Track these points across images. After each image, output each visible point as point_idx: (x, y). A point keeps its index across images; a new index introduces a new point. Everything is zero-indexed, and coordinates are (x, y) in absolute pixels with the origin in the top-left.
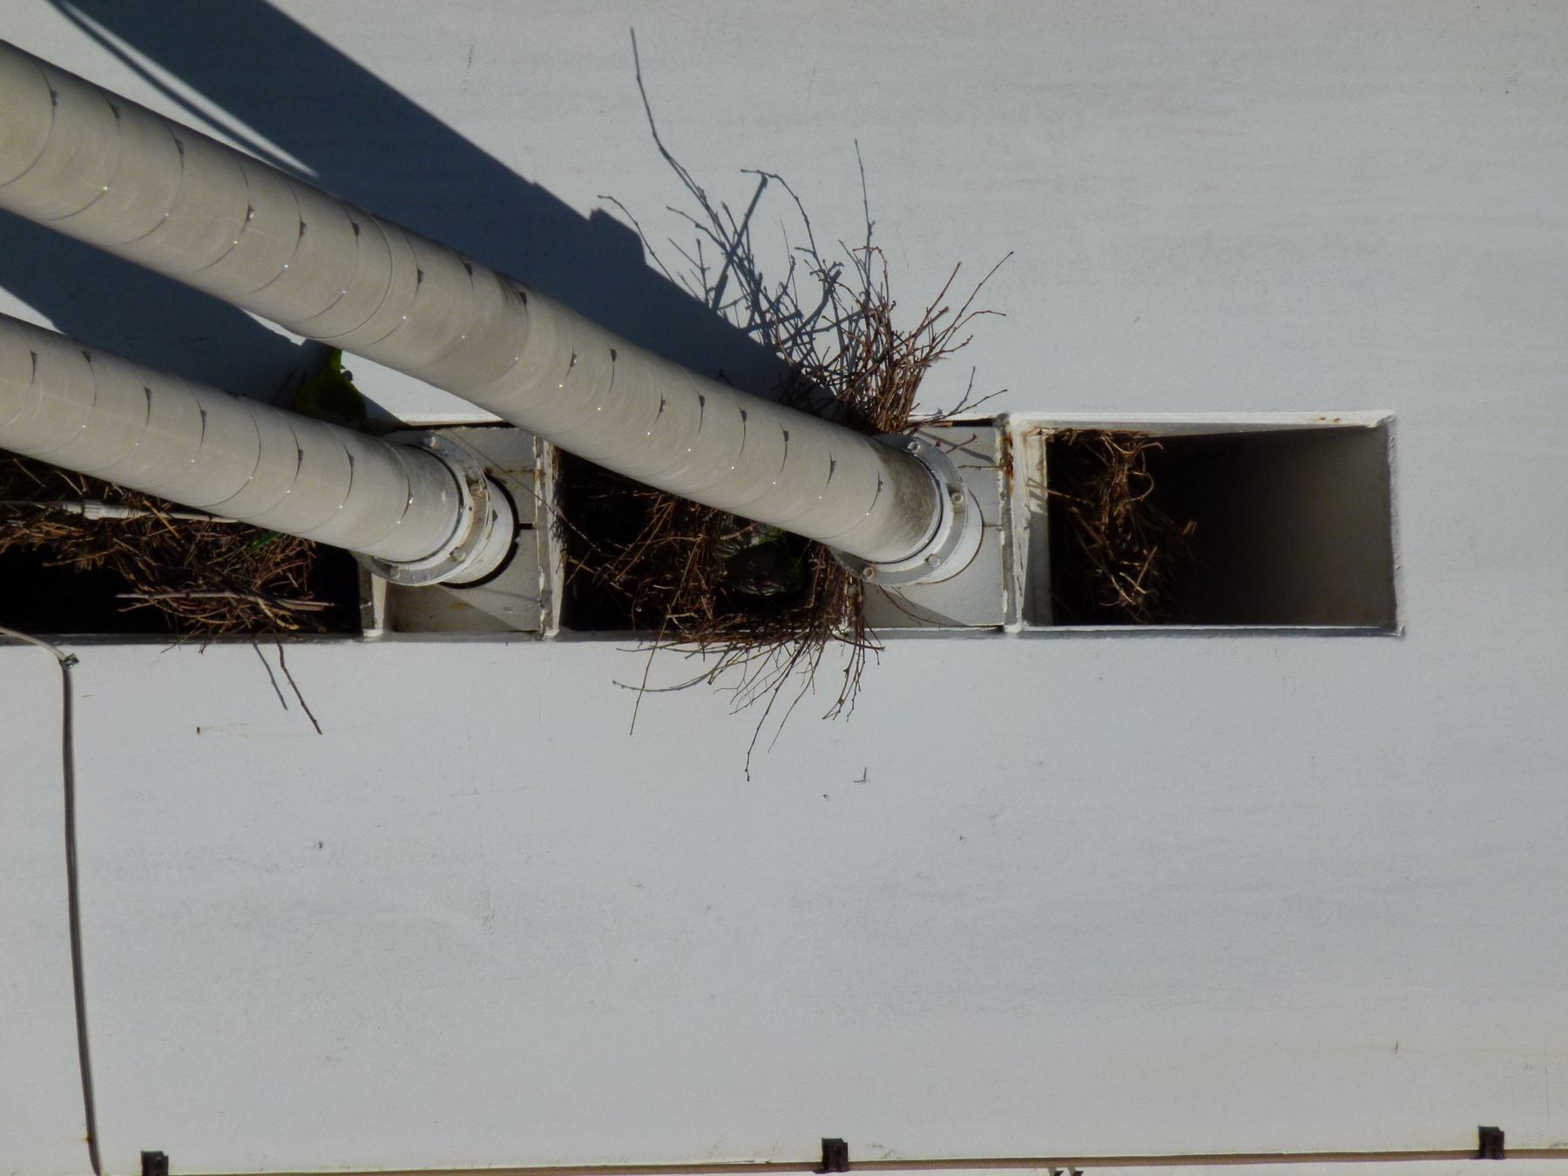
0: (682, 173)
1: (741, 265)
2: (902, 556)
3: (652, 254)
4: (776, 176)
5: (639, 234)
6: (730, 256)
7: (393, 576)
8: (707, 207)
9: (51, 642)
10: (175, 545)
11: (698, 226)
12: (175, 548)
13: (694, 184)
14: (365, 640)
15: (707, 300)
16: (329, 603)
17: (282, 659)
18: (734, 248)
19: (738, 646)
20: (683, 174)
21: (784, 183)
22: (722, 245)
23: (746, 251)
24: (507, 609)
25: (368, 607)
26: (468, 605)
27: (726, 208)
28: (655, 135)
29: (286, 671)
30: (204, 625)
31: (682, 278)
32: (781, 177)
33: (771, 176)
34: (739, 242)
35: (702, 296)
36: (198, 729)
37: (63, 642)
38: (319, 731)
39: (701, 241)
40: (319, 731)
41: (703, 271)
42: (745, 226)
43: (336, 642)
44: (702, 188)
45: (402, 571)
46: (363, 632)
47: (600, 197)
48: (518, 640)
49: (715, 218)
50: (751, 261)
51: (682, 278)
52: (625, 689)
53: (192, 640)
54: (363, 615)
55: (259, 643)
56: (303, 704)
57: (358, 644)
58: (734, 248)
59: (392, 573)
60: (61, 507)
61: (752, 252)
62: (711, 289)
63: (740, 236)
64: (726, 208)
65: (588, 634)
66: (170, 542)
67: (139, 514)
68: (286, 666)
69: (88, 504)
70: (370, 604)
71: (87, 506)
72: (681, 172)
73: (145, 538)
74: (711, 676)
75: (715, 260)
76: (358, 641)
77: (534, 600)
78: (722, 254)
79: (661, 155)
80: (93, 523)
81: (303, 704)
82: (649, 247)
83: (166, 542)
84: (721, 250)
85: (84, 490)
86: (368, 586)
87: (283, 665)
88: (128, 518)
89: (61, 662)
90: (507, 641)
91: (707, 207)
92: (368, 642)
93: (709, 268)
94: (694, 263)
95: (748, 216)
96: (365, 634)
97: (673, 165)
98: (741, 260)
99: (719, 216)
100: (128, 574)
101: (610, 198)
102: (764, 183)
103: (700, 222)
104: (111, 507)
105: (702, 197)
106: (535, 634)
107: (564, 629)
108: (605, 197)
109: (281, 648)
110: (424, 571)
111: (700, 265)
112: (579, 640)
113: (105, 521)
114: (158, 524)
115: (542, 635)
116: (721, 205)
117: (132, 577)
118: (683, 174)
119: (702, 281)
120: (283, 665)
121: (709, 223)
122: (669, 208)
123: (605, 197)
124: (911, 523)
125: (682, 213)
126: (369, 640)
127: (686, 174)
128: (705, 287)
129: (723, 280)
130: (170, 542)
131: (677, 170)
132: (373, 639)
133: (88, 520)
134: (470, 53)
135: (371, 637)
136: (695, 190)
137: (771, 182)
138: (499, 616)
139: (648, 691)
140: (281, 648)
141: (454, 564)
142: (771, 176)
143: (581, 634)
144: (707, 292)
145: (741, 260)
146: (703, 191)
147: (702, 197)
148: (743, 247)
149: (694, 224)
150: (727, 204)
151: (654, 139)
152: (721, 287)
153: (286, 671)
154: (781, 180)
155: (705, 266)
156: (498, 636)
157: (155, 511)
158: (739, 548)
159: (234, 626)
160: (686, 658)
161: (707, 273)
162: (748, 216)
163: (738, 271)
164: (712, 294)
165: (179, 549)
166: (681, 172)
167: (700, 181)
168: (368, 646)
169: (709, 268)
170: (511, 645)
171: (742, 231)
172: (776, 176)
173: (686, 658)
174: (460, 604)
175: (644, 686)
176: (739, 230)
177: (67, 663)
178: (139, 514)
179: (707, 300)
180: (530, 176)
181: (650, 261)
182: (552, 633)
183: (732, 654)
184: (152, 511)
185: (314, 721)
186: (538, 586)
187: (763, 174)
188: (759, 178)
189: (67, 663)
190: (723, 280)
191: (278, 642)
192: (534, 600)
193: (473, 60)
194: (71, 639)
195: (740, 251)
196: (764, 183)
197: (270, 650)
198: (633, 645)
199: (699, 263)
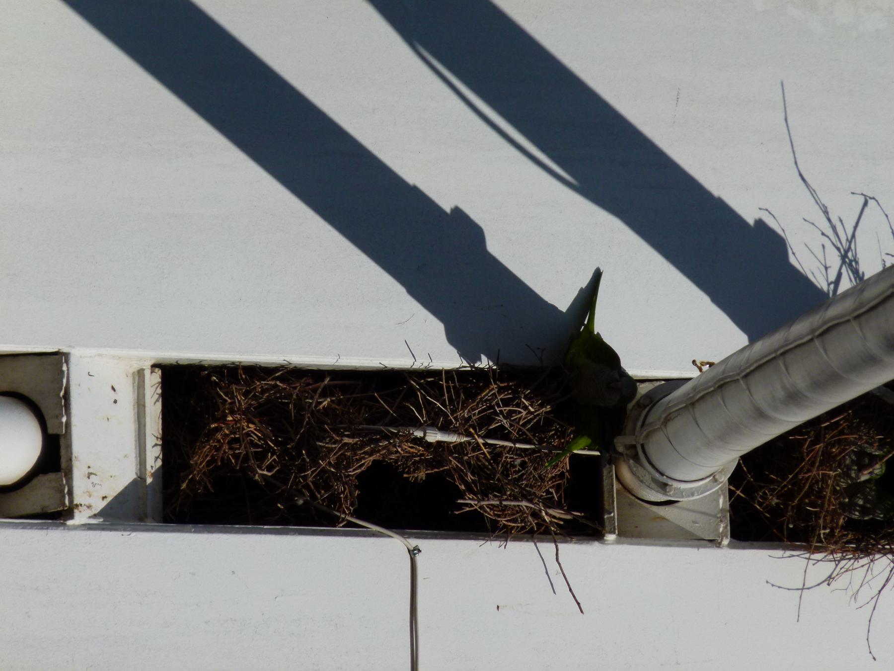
0: (813, 192)
1: (850, 265)
2: (653, 499)
3: (794, 254)
4: (873, 198)
5: (785, 238)
6: (844, 257)
7: (669, 492)
8: (829, 220)
9: (402, 535)
10: (487, 464)
11: (823, 234)
12: (486, 467)
13: (820, 201)
14: (606, 542)
15: (828, 290)
16: (581, 513)
17: (557, 554)
18: (846, 252)
19: (847, 557)
20: (813, 193)
21: (878, 204)
22: (838, 249)
23: (854, 254)
24: (694, 522)
25: (611, 517)
26: (663, 518)
27: (841, 221)
28: (796, 163)
29: (559, 564)
30: (505, 526)
31: (813, 273)
32: (877, 199)
33: (871, 198)
34: (850, 248)
35: (825, 288)
36: (498, 607)
37: (410, 536)
38: (582, 612)
39: (825, 245)
40: (582, 612)
41: (826, 268)
42: (853, 236)
43: (587, 543)
44: (826, 205)
45: (675, 489)
46: (604, 536)
47: (760, 209)
48: (705, 547)
49: (834, 228)
50: (857, 263)
51: (813, 273)
52: (774, 587)
53: (497, 538)
54: (607, 523)
55: (537, 542)
56: (570, 590)
57: (602, 545)
58: (846, 252)
59: (668, 490)
60: (409, 432)
61: (858, 256)
62: (832, 283)
63: (850, 242)
64: (841, 221)
65: (747, 544)
66: (484, 461)
67: (464, 439)
68: (560, 560)
69: (428, 430)
70: (612, 515)
71: (427, 431)
72: (812, 191)
73: (466, 458)
74: (830, 579)
75: (834, 260)
76: (602, 543)
77: (715, 516)
78: (839, 256)
79: (799, 179)
80: (429, 445)
81: (570, 590)
82: (792, 249)
83: (480, 461)
84: (838, 253)
85: (425, 419)
86: (611, 500)
87: (557, 559)
88: (455, 442)
89: (409, 551)
90: (698, 547)
91: (829, 220)
92: (608, 544)
93: (830, 267)
94: (820, 261)
95: (855, 227)
96: (605, 538)
97: (809, 189)
98: (851, 261)
99: (837, 226)
100: (461, 485)
101: (767, 210)
102: (866, 204)
103: (824, 231)
104: (444, 433)
105: (826, 212)
106: (714, 543)
107: (732, 539)
108: (764, 209)
109: (557, 547)
110: (692, 488)
111: (824, 264)
112: (744, 548)
113: (439, 443)
114: (477, 447)
115: (720, 543)
116: (838, 219)
117: (463, 487)
118: (813, 193)
119: (826, 277)
120: (557, 559)
121: (829, 232)
122: (805, 220)
123: (764, 209)
124: (419, 480)
125: (813, 224)
126: (609, 542)
127: (816, 193)
128: (827, 281)
129: (839, 275)
130: (484, 461)
131: (810, 190)
132: (611, 542)
133: (426, 442)
134: (678, 95)
135: (611, 541)
136: (822, 207)
137: (871, 202)
138: (688, 528)
139: (808, 588)
140: (557, 547)
141: (715, 484)
142: (871, 198)
143: (743, 544)
144: (829, 285)
145: (851, 261)
146: (826, 207)
147: (826, 212)
148: (852, 251)
149: (821, 232)
150: (842, 218)
151: (795, 166)
152: (837, 282)
153: (559, 564)
154: (877, 201)
155: (828, 266)
156: (690, 543)
157: (476, 437)
158: (849, 482)
159: (523, 528)
160: (814, 565)
161: (829, 270)
162: (855, 227)
163: (849, 269)
164: (832, 286)
165: (490, 467)
166: (812, 191)
167: (825, 200)
168: (609, 546)
169: (830, 267)
170: (702, 550)
171: (852, 239)
172: (873, 198)
173: (814, 565)
174: (658, 518)
175: (804, 585)
176: (849, 238)
177: (413, 553)
178: (464, 439)
179: (828, 290)
180: (716, 192)
181: (792, 260)
182: (726, 542)
183: (843, 563)
184: (474, 437)
185: (578, 604)
186: (718, 504)
187: (865, 196)
188: (862, 200)
189: (413, 553)
190: (839, 275)
191: (555, 542)
192: (715, 516)
193: (679, 100)
194: (415, 533)
195: (850, 255)
196: (866, 204)
197: (548, 548)
198: (779, 553)
199: (823, 262)
